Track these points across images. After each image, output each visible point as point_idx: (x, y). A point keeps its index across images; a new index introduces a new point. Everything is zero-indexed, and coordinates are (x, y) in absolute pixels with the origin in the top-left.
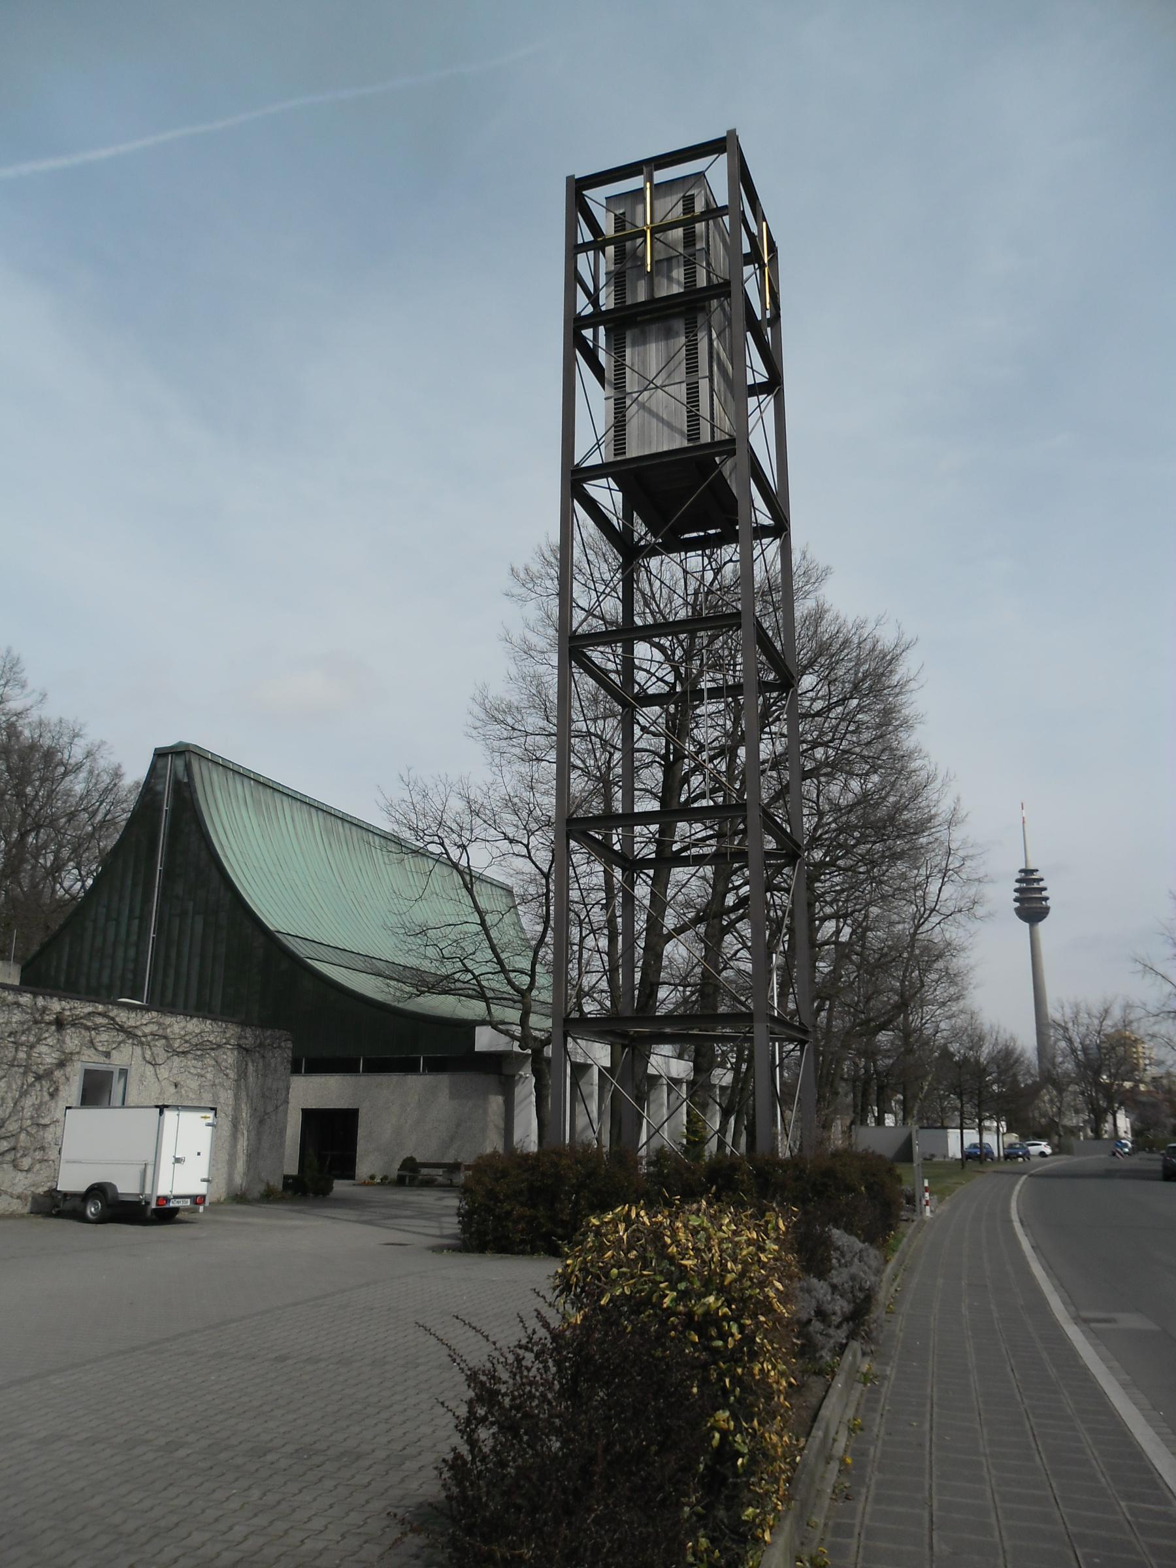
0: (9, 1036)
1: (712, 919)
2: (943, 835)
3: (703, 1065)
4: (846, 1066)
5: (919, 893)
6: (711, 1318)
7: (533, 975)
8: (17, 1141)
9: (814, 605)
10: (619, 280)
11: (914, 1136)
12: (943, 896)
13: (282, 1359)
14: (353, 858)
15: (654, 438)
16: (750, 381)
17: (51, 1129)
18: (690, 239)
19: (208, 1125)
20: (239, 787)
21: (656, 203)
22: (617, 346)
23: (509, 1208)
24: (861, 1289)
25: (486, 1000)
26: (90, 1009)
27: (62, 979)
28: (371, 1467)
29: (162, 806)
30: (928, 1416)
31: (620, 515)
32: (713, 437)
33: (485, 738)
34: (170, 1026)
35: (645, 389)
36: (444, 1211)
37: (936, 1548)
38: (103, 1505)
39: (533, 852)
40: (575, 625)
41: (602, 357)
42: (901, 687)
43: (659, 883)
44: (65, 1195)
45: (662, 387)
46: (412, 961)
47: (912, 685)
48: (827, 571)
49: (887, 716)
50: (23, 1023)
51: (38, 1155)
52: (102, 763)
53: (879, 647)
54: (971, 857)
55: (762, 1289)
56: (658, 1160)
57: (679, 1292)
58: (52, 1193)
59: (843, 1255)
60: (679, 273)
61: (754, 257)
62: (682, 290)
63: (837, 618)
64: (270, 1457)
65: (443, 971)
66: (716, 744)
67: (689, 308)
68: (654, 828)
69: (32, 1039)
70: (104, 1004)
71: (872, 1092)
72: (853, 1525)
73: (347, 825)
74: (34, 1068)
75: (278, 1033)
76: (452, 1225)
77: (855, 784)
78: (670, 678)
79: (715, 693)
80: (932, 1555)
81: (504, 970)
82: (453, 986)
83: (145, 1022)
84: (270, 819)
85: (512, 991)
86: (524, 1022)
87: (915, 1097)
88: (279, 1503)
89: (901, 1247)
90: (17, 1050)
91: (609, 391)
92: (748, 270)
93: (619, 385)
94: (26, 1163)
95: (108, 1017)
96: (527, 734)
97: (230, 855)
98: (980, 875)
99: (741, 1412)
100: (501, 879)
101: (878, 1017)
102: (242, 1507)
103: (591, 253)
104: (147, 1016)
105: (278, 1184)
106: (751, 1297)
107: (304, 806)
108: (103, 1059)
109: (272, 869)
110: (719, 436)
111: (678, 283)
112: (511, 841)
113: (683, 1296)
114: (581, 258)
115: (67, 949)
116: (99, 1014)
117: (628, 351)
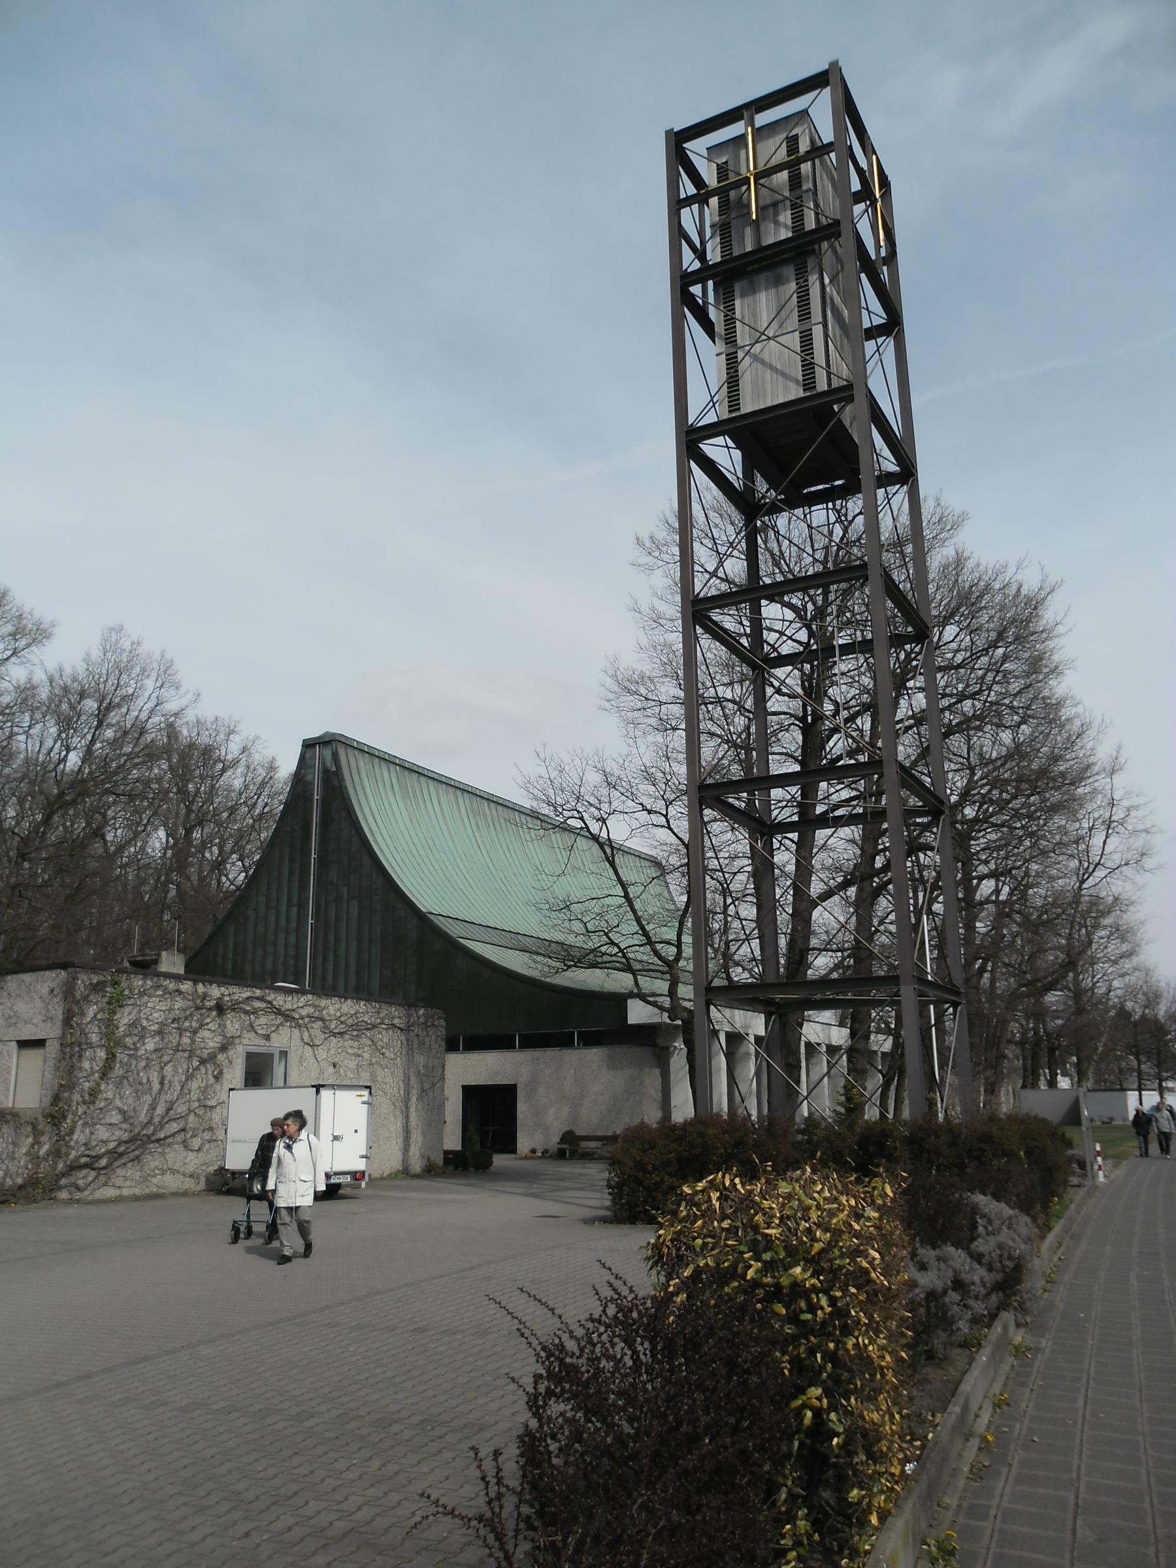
0: (173, 1022)
1: (863, 880)
2: (1102, 782)
3: (859, 1033)
4: (1014, 1027)
5: (1082, 847)
6: (798, 1290)
7: (679, 945)
8: (187, 1123)
9: (953, 553)
10: (724, 230)
11: (1082, 1101)
12: (1108, 849)
13: (421, 1330)
14: (501, 837)
15: (770, 388)
16: (866, 324)
17: (218, 1110)
18: (795, 181)
19: (364, 1103)
20: (385, 773)
21: (759, 147)
22: (726, 299)
23: (658, 1179)
24: (1010, 1258)
25: (634, 973)
26: (248, 994)
27: (229, 966)
28: (491, 1438)
29: (312, 795)
30: (1083, 1391)
31: (740, 475)
32: (829, 384)
33: (619, 709)
34: (325, 1008)
35: (757, 342)
36: (591, 1186)
37: (1079, 1535)
38: (229, 1472)
39: (671, 822)
40: (697, 591)
41: (713, 313)
42: (1048, 633)
43: (804, 850)
44: (233, 1173)
45: (774, 338)
46: (558, 936)
47: (1060, 629)
48: (963, 517)
49: (1036, 665)
50: (185, 1010)
51: (207, 1136)
52: (257, 757)
53: (1024, 592)
54: (1137, 807)
55: (853, 1260)
56: (807, 1127)
57: (765, 1263)
58: (222, 1170)
59: (990, 1222)
60: (786, 217)
61: (865, 194)
62: (790, 235)
63: (978, 565)
64: (395, 1428)
65: (590, 945)
66: (853, 702)
67: (799, 253)
68: (794, 790)
69: (194, 1024)
70: (261, 989)
71: (1042, 1057)
72: (990, 1507)
73: (492, 805)
74: (198, 1052)
75: (431, 1012)
76: (601, 1200)
77: (1006, 736)
78: (803, 636)
79: (846, 649)
80: (1074, 1542)
81: (650, 942)
82: (599, 960)
83: (302, 1005)
84: (417, 803)
85: (660, 963)
86: (672, 993)
87: (1089, 1059)
88: (396, 1474)
89: (1067, 1213)
90: (181, 1035)
91: (721, 346)
92: (859, 208)
93: (730, 339)
94: (196, 1143)
95: (266, 1001)
96: (661, 704)
97: (380, 840)
98: (1148, 825)
99: (836, 1390)
100: (646, 850)
101: (1046, 977)
102: (361, 1477)
103: (695, 207)
104: (303, 1000)
105: (439, 1160)
106: (841, 1267)
107: (451, 790)
108: (263, 1042)
109: (422, 853)
110: (836, 383)
111: (786, 226)
112: (649, 812)
113: (769, 1267)
114: (685, 213)
115: (232, 936)
116: (257, 998)
117: (738, 303)
